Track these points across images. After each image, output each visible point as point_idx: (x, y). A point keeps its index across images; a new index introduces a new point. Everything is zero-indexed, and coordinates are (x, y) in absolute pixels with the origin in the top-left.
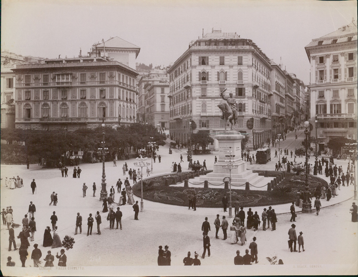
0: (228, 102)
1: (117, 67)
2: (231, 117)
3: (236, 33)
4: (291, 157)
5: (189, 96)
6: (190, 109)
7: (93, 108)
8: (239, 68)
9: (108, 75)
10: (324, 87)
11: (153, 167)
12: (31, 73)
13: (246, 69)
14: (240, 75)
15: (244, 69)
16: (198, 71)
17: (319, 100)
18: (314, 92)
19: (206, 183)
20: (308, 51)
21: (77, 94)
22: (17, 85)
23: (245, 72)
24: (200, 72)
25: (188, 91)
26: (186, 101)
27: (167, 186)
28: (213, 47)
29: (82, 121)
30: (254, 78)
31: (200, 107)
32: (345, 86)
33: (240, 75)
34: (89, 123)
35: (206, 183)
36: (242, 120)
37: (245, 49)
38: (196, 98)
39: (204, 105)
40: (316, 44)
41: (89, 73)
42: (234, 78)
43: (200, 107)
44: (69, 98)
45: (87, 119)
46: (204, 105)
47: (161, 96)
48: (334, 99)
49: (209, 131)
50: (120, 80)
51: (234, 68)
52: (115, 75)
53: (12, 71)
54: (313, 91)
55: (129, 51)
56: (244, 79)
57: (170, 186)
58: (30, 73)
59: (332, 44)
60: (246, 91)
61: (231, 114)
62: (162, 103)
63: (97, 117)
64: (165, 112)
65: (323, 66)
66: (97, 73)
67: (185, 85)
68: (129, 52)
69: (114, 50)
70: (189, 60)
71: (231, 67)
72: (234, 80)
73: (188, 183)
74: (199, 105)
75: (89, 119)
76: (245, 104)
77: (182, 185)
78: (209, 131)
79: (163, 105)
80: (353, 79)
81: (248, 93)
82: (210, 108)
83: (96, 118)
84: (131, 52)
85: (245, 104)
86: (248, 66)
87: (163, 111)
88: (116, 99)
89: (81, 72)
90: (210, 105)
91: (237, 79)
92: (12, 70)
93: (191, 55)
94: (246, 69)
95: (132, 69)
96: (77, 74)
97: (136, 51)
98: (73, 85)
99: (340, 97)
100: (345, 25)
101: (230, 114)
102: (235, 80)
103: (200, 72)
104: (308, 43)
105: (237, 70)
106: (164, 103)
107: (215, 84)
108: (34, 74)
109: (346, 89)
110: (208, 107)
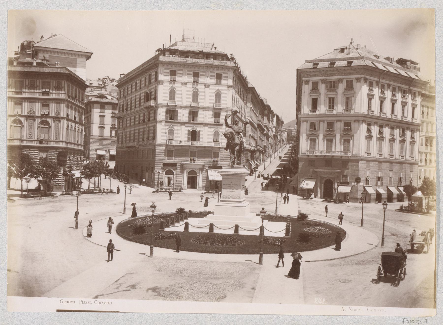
0: (234, 131)
2: (237, 148)
3: (213, 44)
4: (170, 199)
5: (152, 119)
6: (151, 135)
7: (31, 127)
8: (217, 88)
9: (54, 85)
10: (394, 123)
13: (225, 90)
14: (218, 96)
15: (222, 90)
17: (311, 133)
18: (305, 123)
20: (300, 73)
21: (53, 110)
22: (8, 93)
23: (224, 93)
25: (149, 113)
26: (147, 124)
27: (163, 229)
30: (233, 102)
31: (165, 133)
32: (378, 121)
33: (218, 96)
37: (226, 65)
39: (171, 132)
40: (311, 66)
41: (27, 80)
42: (210, 100)
43: (165, 133)
46: (171, 132)
47: (100, 116)
48: (311, 133)
49: (176, 164)
51: (210, 87)
52: (63, 85)
54: (304, 121)
55: (78, 55)
57: (167, 229)
59: (329, 67)
60: (179, 115)
61: (238, 145)
62: (101, 125)
63: (36, 139)
64: (103, 136)
65: (334, 93)
67: (147, 104)
69: (58, 52)
70: (154, 73)
72: (164, 100)
73: (214, 226)
74: (164, 131)
76: (199, 131)
78: (176, 164)
79: (102, 128)
81: (181, 116)
82: (178, 135)
83: (35, 141)
85: (199, 131)
86: (228, 87)
87: (102, 136)
88: (63, 118)
90: (179, 132)
93: (157, 67)
94: (225, 90)
96: (38, 81)
97: (87, 55)
99: (335, 132)
100: (343, 46)
101: (236, 145)
102: (189, 102)
104: (301, 64)
105: (214, 91)
106: (103, 125)
109: (326, 122)
110: (176, 134)
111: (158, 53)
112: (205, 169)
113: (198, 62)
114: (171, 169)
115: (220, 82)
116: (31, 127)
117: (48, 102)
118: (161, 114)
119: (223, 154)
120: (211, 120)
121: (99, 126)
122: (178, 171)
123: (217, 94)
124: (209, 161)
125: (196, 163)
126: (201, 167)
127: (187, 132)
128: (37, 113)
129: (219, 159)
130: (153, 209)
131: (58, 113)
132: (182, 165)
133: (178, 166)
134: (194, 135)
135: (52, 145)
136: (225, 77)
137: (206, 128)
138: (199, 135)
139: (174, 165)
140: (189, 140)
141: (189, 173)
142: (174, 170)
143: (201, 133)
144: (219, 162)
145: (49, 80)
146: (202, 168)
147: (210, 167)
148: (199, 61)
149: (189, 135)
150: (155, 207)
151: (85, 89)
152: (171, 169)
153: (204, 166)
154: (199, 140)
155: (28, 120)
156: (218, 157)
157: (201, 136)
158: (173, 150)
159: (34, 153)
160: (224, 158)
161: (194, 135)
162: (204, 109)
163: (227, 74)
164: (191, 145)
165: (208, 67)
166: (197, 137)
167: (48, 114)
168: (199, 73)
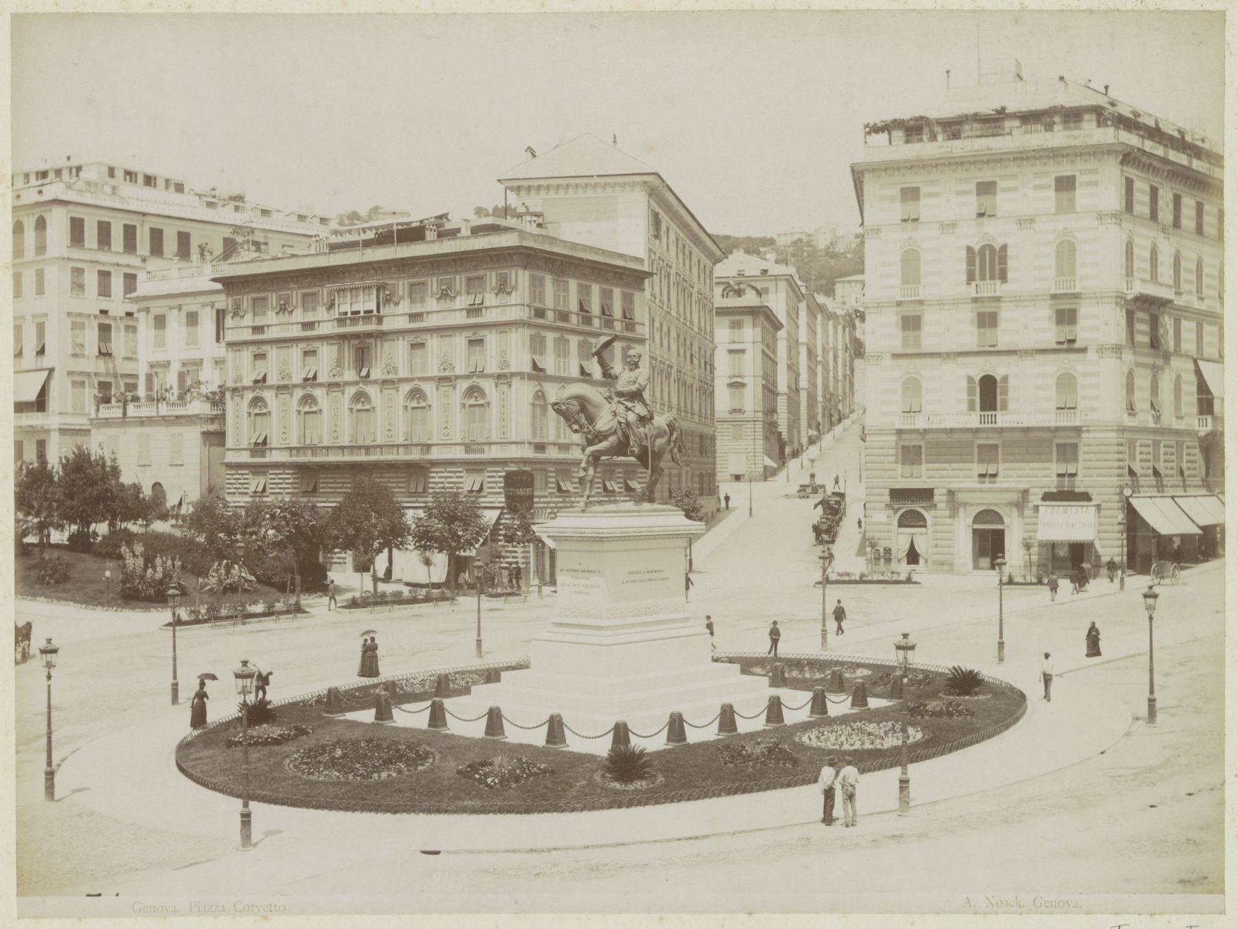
1: (520, 254)
7: (446, 408)
9: (494, 284)
11: (1005, 639)
12: (428, 275)
14: (1066, 253)
16: (964, 243)
19: (494, 719)
24: (969, 250)
28: (940, 147)
29: (415, 455)
33: (1066, 253)
34: (434, 463)
35: (494, 719)
36: (1075, 446)
38: (879, 357)
39: (912, 387)
41: (435, 279)
44: (377, 374)
45: (427, 447)
46: (912, 387)
50: (542, 300)
53: (219, 286)
56: (1080, 271)
58: (264, 291)
66: (458, 277)
68: (618, 189)
71: (1025, 222)
75: (434, 449)
76: (1005, 378)
77: (367, 716)
80: (1077, 282)
83: (398, 446)
84: (628, 188)
89: (413, 277)
91: (897, 281)
92: (214, 280)
95: (621, 256)
98: (387, 326)
103: (969, 250)
106: (740, 380)
107: (956, 303)
108: (275, 291)
111: (1176, 134)
112: (1031, 505)
113: (989, 149)
114: (917, 507)
115: (1072, 202)
116: (446, 408)
117: (482, 333)
118: (880, 333)
119: (1093, 449)
120: (1049, 334)
121: (729, 381)
122: (939, 513)
123: (1061, 245)
124: (1045, 475)
125: (997, 485)
126: (1014, 497)
127: (964, 384)
128: (294, 375)
129: (1079, 467)
130: (1151, 601)
131: (285, 375)
132: (951, 493)
133: (939, 497)
134: (989, 392)
135: (494, 453)
136: (1089, 184)
137: (1028, 364)
138: (1005, 392)
139: (926, 494)
140: (971, 407)
141: (978, 518)
142: (927, 508)
143: (1011, 383)
144: (1079, 478)
145: (482, 272)
146: (1021, 501)
147: (1048, 497)
148: (992, 146)
149: (971, 392)
150: (1155, 596)
151: (643, 283)
152: (917, 507)
153: (1025, 492)
154: (1004, 408)
155: (442, 389)
156: (1075, 460)
157: (1011, 394)
158: (920, 447)
159: (455, 480)
160: (1098, 464)
161: (989, 392)
162: (1098, 298)
163: (1096, 171)
164: (977, 425)
165: (1022, 157)
166: (999, 398)
167: (315, 378)
168: (1074, 177)
